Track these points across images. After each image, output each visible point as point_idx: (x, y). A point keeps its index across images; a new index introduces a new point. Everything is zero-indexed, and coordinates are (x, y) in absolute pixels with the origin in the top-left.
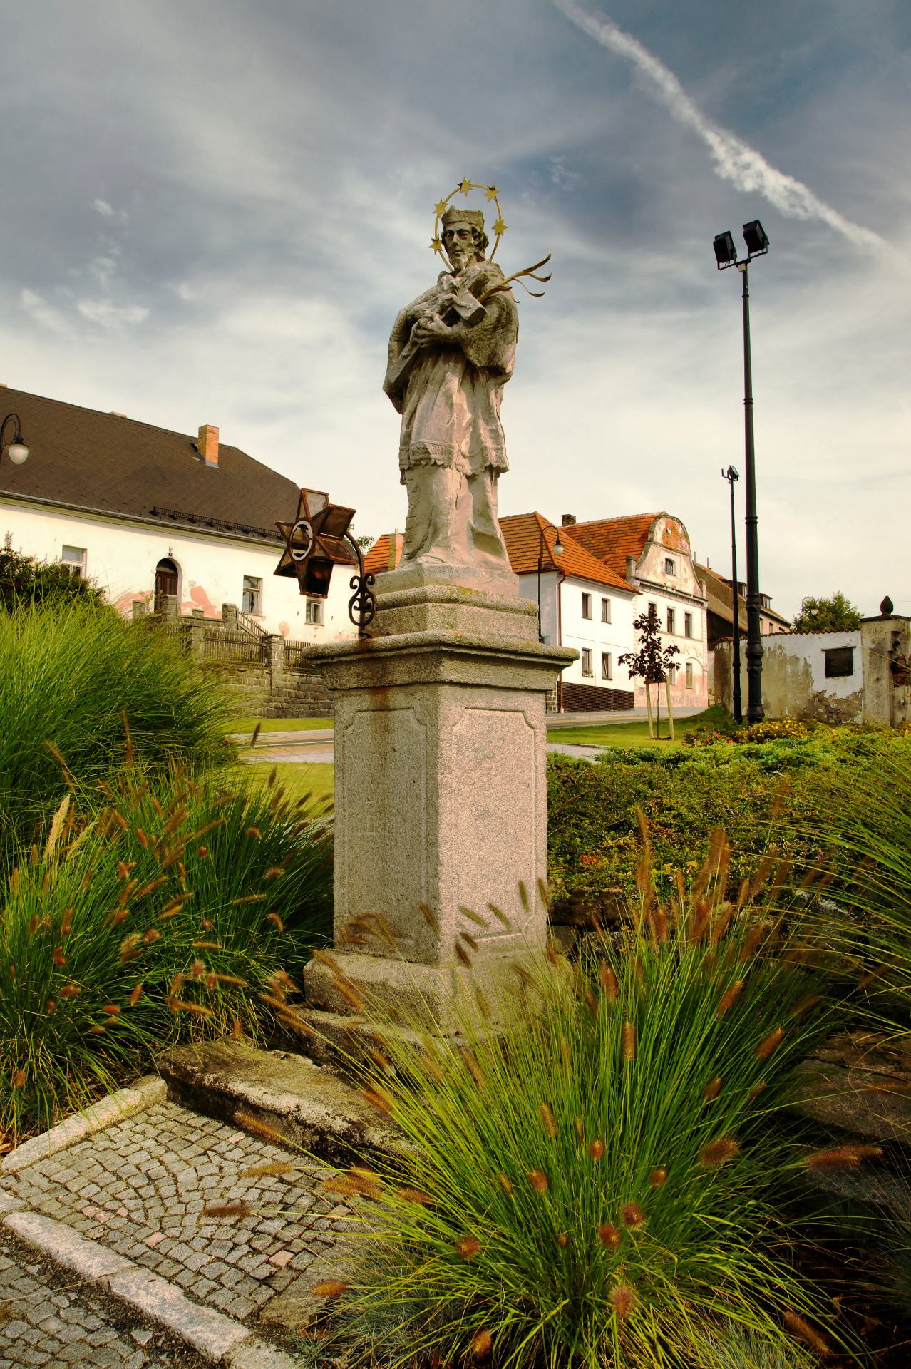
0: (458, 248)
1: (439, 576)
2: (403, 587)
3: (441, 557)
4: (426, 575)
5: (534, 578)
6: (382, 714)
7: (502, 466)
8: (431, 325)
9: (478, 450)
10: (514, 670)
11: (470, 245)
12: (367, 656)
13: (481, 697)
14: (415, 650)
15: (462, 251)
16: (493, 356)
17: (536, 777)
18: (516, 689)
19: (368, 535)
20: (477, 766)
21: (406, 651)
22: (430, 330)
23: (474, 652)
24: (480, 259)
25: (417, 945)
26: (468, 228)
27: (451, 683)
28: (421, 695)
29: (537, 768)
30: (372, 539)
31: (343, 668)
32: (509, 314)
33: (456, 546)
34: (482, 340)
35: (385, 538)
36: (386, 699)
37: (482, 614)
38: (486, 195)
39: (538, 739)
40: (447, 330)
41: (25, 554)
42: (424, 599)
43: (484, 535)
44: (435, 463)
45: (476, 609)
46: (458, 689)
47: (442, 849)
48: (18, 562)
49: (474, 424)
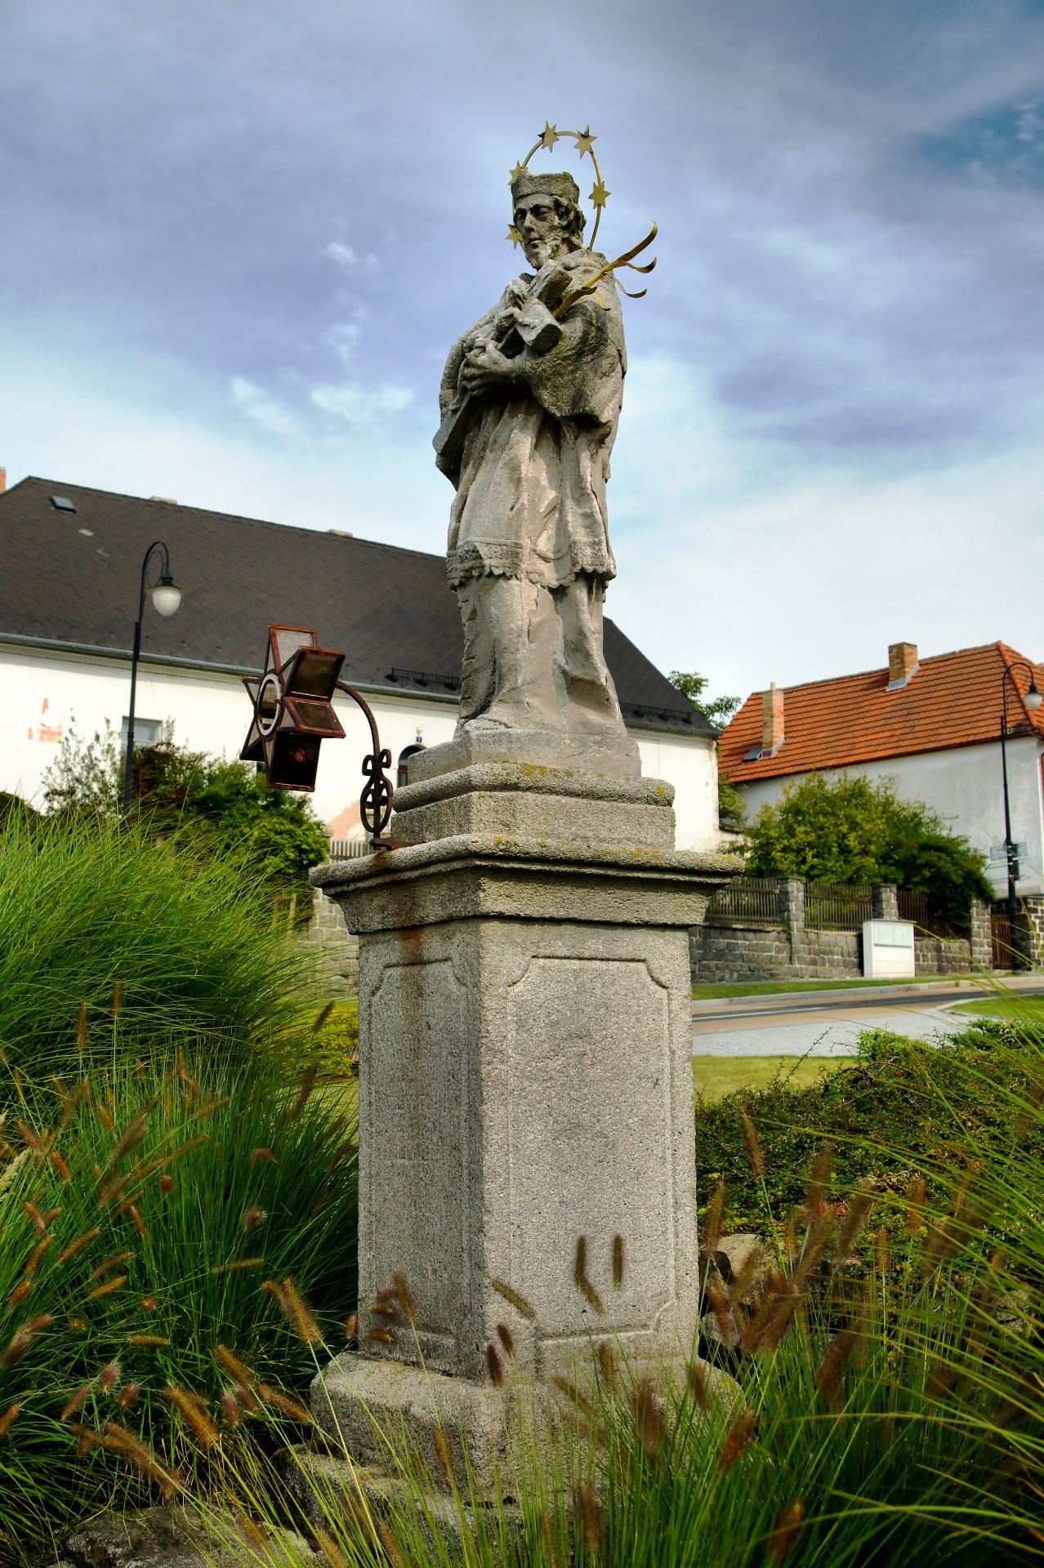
0: (534, 235)
1: (493, 749)
2: (447, 769)
3: (504, 720)
4: (474, 749)
5: (995, 750)
6: (415, 969)
7: (601, 570)
8: (482, 359)
9: (565, 550)
10: (620, 893)
11: (552, 228)
12: (387, 879)
13: (561, 940)
14: (442, 867)
15: (541, 238)
16: (579, 397)
17: (673, 1068)
18: (627, 925)
19: (731, 694)
20: (557, 1052)
21: (432, 870)
22: (479, 367)
23: (538, 867)
24: (573, 248)
25: (458, 1346)
26: (547, 201)
27: (501, 917)
28: (461, 935)
29: (673, 1052)
30: (738, 700)
31: (364, 898)
32: (601, 330)
33: (534, 701)
34: (561, 375)
35: (756, 698)
36: (419, 945)
37: (563, 806)
38: (576, 147)
39: (675, 1005)
40: (506, 364)
41: (194, 748)
42: (467, 787)
43: (582, 680)
44: (491, 574)
45: (552, 798)
46: (517, 927)
47: (490, 1187)
48: (182, 762)
49: (558, 507)
